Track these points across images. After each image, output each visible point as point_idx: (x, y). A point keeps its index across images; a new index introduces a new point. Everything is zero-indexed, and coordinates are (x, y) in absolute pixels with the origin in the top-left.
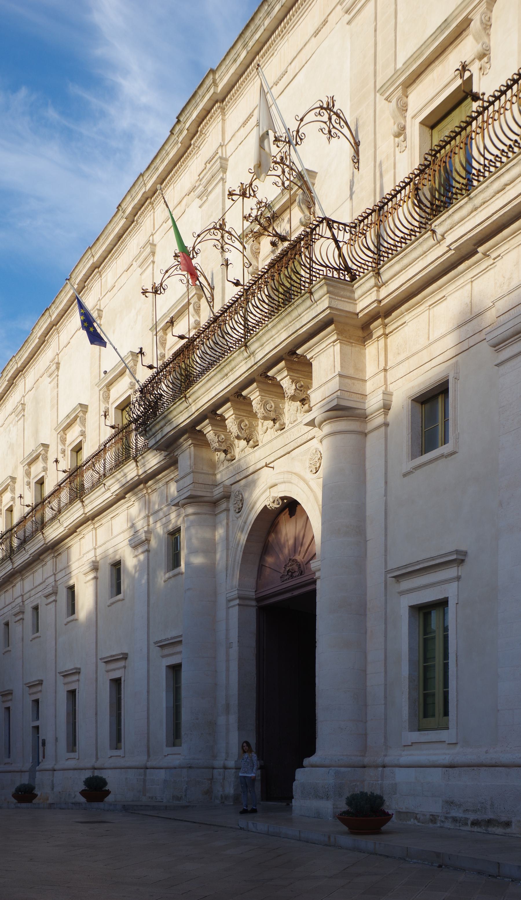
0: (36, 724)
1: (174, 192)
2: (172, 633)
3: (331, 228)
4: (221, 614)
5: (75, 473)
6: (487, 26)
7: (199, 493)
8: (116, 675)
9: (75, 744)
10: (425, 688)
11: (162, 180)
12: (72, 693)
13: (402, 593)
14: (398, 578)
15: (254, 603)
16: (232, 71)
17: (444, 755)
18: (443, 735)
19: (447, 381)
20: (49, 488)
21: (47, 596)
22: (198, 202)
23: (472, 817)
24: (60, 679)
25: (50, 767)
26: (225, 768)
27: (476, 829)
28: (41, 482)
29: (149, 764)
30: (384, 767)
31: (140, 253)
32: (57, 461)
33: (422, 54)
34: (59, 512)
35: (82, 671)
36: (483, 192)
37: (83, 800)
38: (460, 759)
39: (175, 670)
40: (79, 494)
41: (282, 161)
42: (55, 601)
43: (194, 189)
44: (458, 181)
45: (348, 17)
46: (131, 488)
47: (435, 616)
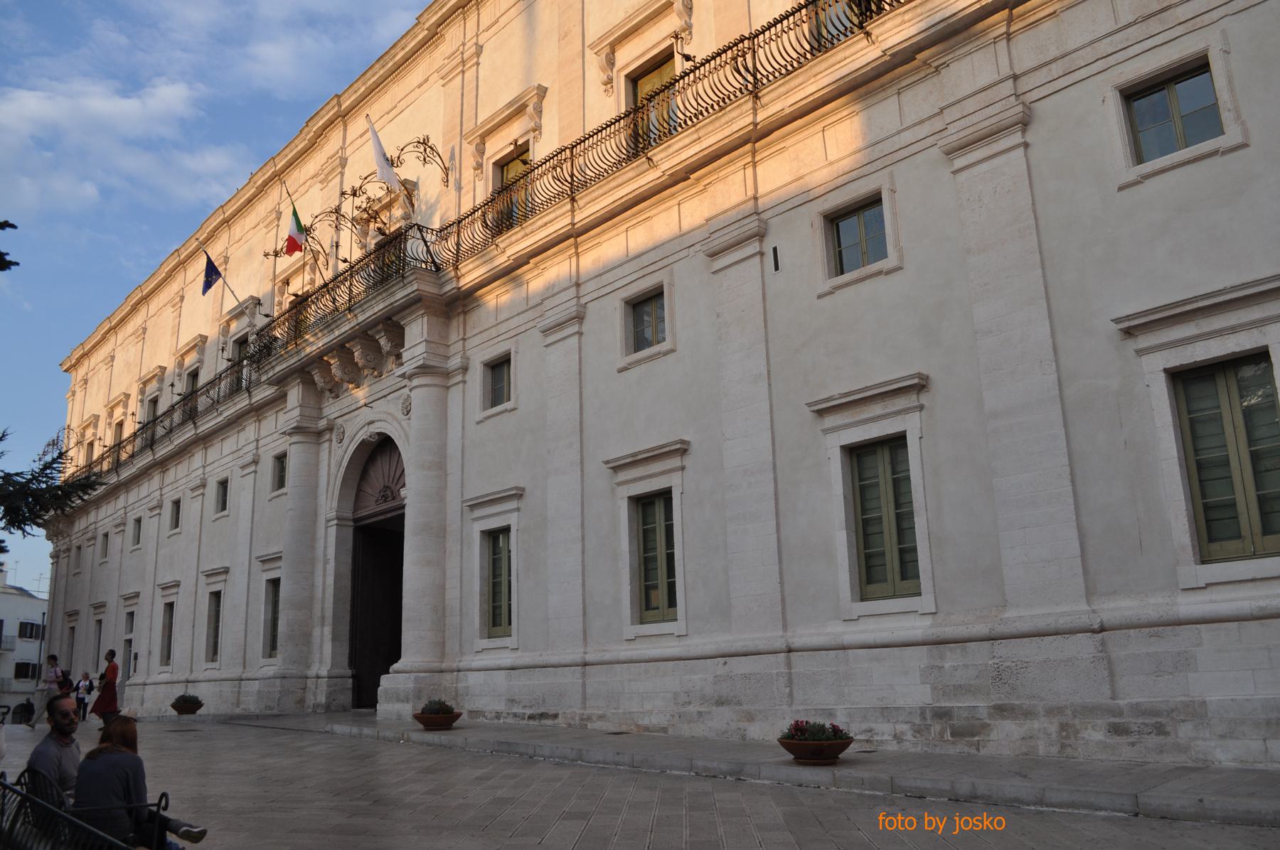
0: (128, 637)
1: (297, 177)
2: (273, 549)
3: (421, 231)
4: (321, 532)
5: (190, 397)
6: (539, 112)
7: (305, 425)
8: (215, 588)
9: (169, 658)
10: (494, 601)
11: (289, 165)
12: (170, 606)
13: (475, 520)
14: (472, 507)
15: (351, 523)
16: (353, 98)
17: (507, 659)
18: (506, 641)
19: (880, 193)
20: (162, 407)
21: (151, 509)
22: (319, 186)
23: (529, 712)
24: (159, 592)
25: (141, 681)
26: (318, 677)
27: (531, 722)
28: (154, 402)
29: (244, 676)
30: (459, 671)
31: (267, 217)
32: (172, 385)
33: (632, 20)
34: (171, 431)
35: (694, 448)
36: (535, 222)
37: (174, 713)
38: (519, 662)
39: (275, 583)
40: (191, 415)
41: (424, 143)
42: (203, 494)
43: (316, 175)
44: (518, 212)
45: (442, 82)
46: (859, 87)
47: (659, 509)
